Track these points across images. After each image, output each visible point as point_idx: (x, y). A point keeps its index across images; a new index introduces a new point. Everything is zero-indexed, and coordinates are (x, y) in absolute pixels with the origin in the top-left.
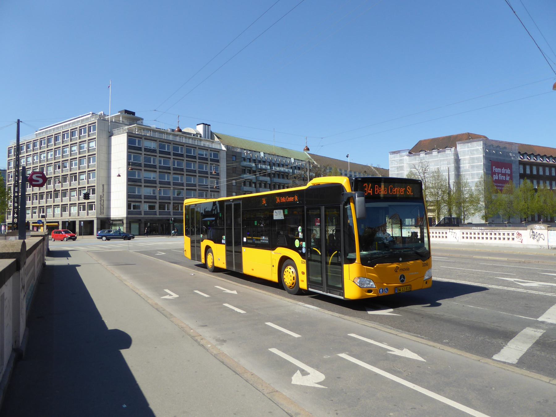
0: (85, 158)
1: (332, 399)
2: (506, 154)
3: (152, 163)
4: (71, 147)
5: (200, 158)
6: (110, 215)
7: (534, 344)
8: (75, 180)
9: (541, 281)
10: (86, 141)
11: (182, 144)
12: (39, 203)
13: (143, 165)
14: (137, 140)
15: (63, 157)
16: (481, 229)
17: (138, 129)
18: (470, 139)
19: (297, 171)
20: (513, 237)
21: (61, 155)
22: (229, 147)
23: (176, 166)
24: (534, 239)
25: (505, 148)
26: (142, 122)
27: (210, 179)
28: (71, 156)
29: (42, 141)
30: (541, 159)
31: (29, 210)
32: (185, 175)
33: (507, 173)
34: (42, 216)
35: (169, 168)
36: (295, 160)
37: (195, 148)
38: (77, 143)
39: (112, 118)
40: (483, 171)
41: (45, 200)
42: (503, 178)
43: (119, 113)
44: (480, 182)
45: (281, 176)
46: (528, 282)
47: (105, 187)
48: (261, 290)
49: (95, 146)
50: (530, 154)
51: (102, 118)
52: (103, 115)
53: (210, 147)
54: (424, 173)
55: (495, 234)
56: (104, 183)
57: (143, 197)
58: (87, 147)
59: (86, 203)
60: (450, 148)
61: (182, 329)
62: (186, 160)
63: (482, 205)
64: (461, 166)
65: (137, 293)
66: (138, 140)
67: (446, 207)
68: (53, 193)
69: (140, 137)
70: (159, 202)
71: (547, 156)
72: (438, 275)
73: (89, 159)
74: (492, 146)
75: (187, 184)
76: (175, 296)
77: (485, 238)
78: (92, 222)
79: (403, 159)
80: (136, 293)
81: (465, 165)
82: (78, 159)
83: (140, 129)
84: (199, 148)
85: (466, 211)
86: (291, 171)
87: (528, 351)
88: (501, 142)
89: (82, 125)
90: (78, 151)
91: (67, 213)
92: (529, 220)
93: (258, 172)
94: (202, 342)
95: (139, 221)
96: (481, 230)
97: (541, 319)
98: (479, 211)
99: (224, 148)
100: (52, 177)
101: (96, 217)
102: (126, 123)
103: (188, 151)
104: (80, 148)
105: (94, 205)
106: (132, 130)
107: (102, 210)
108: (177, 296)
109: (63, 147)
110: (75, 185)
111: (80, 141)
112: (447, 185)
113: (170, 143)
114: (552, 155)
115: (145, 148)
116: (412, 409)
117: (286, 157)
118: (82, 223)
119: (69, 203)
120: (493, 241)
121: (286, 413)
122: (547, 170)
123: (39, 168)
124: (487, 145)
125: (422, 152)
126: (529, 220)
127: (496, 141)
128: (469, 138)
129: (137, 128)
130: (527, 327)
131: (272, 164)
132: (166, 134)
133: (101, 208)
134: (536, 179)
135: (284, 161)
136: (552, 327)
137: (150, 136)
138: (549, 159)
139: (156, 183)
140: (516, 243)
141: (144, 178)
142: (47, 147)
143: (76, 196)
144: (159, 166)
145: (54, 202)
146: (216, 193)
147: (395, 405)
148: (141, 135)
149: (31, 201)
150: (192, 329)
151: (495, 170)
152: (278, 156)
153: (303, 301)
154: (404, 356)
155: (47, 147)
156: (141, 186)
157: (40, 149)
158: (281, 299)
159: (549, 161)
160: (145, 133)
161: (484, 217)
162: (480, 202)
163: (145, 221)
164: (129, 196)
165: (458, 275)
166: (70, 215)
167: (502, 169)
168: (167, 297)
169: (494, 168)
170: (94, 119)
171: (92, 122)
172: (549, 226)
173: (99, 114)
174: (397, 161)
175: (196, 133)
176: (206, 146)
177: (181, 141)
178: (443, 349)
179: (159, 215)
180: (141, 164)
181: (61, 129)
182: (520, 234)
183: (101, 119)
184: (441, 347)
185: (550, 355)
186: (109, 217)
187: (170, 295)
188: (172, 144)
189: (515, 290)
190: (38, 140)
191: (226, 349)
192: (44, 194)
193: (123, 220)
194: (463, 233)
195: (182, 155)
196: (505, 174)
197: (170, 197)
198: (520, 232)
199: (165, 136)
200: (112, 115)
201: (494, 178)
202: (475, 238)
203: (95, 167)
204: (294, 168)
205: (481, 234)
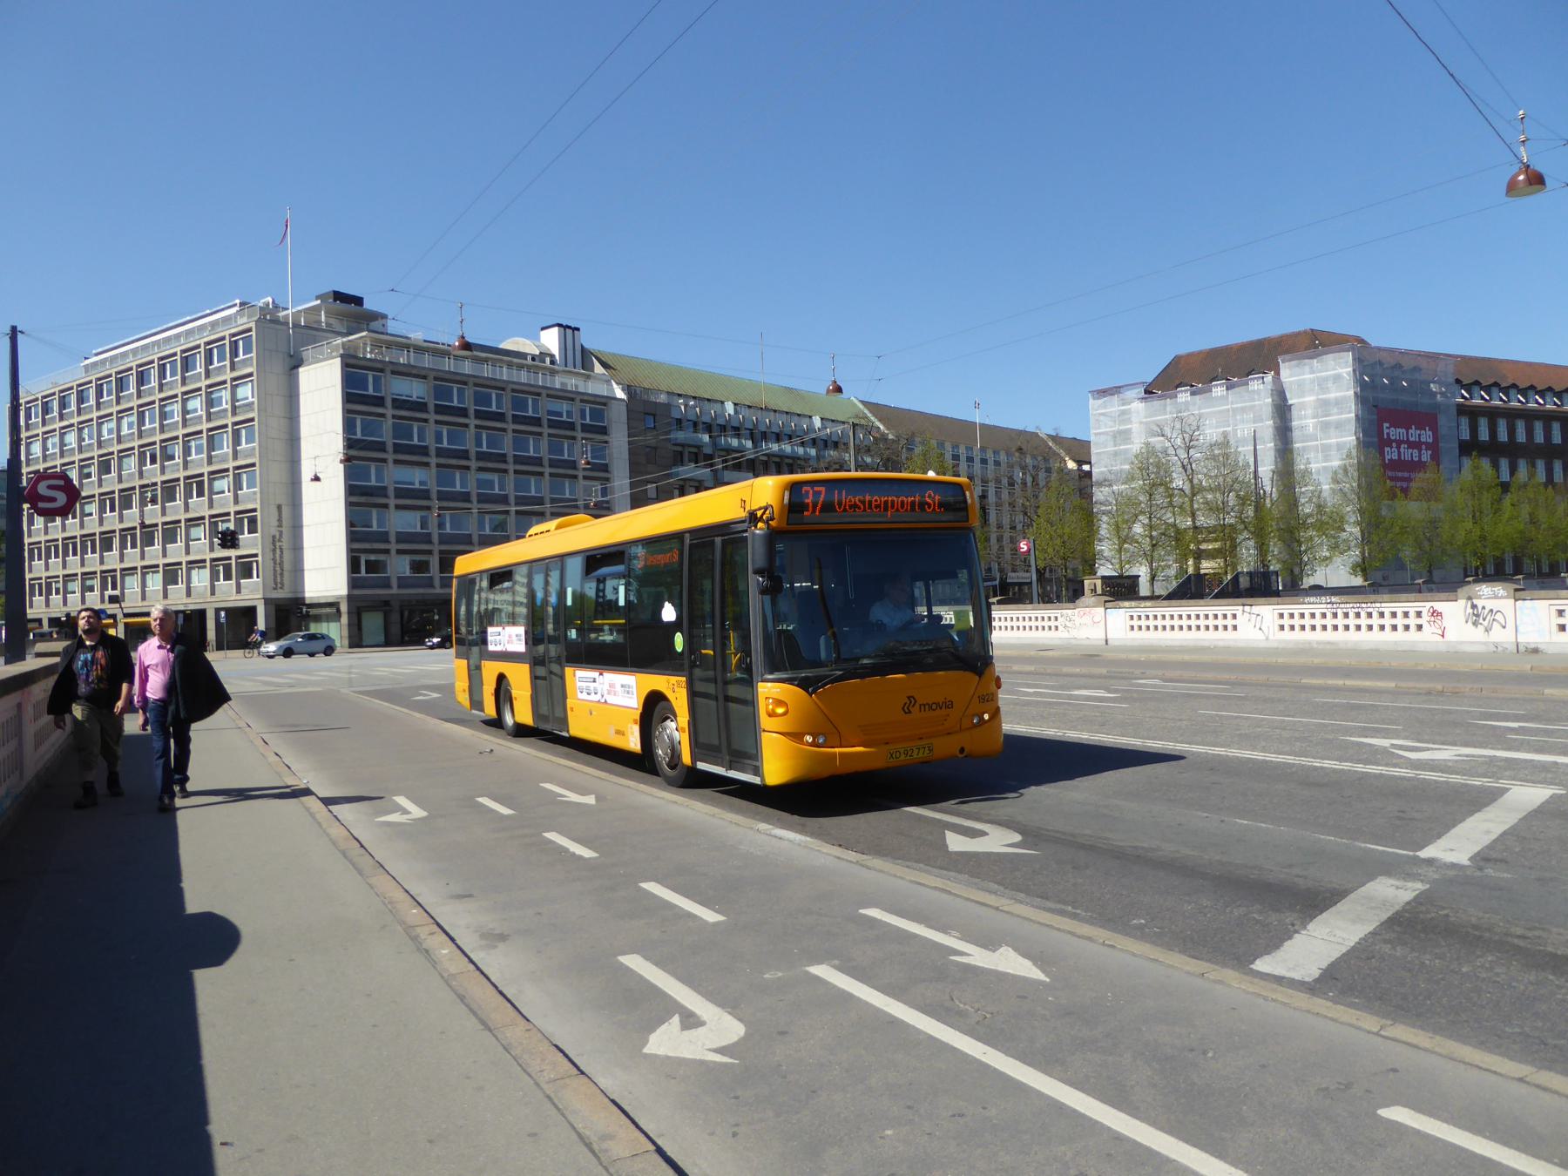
0: (226, 432)
2: (1420, 387)
3: (416, 441)
4: (185, 402)
5: (552, 424)
6: (304, 592)
7: (1382, 924)
8: (201, 494)
9: (1466, 745)
10: (224, 382)
11: (499, 384)
12: (102, 562)
13: (390, 448)
14: (370, 375)
15: (162, 430)
16: (1329, 601)
17: (372, 345)
18: (1316, 347)
19: (832, 452)
20: (1419, 621)
21: (157, 425)
22: (635, 391)
24: (1477, 626)
25: (1416, 369)
26: (384, 325)
27: (582, 482)
28: (185, 425)
29: (102, 385)
30: (1521, 399)
31: (74, 580)
32: (511, 472)
33: (1422, 440)
34: (110, 597)
35: (464, 455)
37: (539, 394)
38: (199, 389)
39: (297, 315)
40: (1354, 438)
41: (118, 553)
42: (1412, 457)
43: (317, 299)
44: (1345, 470)
46: (1428, 749)
47: (286, 511)
49: (253, 397)
50: (1544, 390)
51: (268, 317)
52: (271, 307)
54: (1189, 448)
55: (1370, 615)
56: (282, 498)
57: (393, 538)
58: (229, 397)
59: (234, 559)
60: (1261, 375)
61: (389, 906)
62: (514, 431)
63: (1351, 533)
64: (1293, 423)
66: (373, 375)
67: (1251, 543)
68: (138, 531)
69: (378, 368)
70: (441, 552)
71: (1502, 386)
72: (1181, 735)
73: (236, 434)
74: (1381, 363)
77: (1388, 628)
78: (251, 611)
79: (1130, 409)
81: (1304, 422)
82: (204, 435)
83: (377, 345)
84: (548, 396)
85: (1306, 551)
86: (813, 452)
87: (1358, 946)
89: (213, 337)
90: (204, 413)
91: (182, 586)
92: (1488, 573)
95: (384, 605)
96: (1329, 606)
97: (1426, 853)
98: (1345, 551)
99: (620, 394)
100: (134, 488)
101: (261, 596)
103: (519, 404)
104: (210, 403)
105: (255, 564)
106: (356, 349)
107: (279, 576)
108: (424, 814)
109: (162, 400)
110: (199, 506)
111: (209, 382)
112: (1253, 481)
114: (1535, 384)
116: (953, 1118)
117: (799, 415)
118: (223, 614)
119: (184, 559)
120: (1364, 635)
122: (1538, 428)
123: (96, 464)
124: (1366, 363)
125: (1183, 388)
126: (1488, 573)
127: (1391, 351)
128: (1314, 343)
129: (369, 343)
130: (1380, 877)
131: (758, 435)
133: (275, 570)
134: (1506, 457)
135: (793, 424)
136: (1452, 873)
137: (409, 365)
138: (1543, 397)
140: (1428, 638)
141: (396, 483)
142: (118, 403)
143: (203, 540)
144: (437, 448)
145: (143, 558)
147: (909, 1107)
148: (381, 361)
149: (78, 557)
151: (1388, 434)
152: (775, 411)
154: (993, 968)
155: (118, 403)
156: (386, 506)
157: (98, 408)
158: (714, 816)
159: (1542, 402)
160: (394, 356)
161: (1358, 569)
162: (1346, 526)
165: (1240, 735)
166: (189, 594)
167: (1410, 431)
168: (394, 818)
169: (1387, 428)
170: (245, 320)
171: (240, 328)
172: (1518, 587)
174: (1111, 417)
175: (541, 353)
176: (569, 388)
177: (498, 378)
179: (399, 587)
181: (156, 351)
182: (1440, 614)
183: (265, 318)
184: (1109, 939)
185: (1417, 954)
186: (299, 596)
187: (405, 812)
188: (471, 384)
189: (1383, 772)
190: (90, 382)
192: (115, 536)
193: (338, 603)
194: (1281, 616)
195: (500, 417)
196: (1416, 445)
198: (1439, 606)
199: (449, 363)
200: (297, 306)
201: (1388, 457)
202: (1303, 628)
204: (821, 444)
205: (1329, 615)
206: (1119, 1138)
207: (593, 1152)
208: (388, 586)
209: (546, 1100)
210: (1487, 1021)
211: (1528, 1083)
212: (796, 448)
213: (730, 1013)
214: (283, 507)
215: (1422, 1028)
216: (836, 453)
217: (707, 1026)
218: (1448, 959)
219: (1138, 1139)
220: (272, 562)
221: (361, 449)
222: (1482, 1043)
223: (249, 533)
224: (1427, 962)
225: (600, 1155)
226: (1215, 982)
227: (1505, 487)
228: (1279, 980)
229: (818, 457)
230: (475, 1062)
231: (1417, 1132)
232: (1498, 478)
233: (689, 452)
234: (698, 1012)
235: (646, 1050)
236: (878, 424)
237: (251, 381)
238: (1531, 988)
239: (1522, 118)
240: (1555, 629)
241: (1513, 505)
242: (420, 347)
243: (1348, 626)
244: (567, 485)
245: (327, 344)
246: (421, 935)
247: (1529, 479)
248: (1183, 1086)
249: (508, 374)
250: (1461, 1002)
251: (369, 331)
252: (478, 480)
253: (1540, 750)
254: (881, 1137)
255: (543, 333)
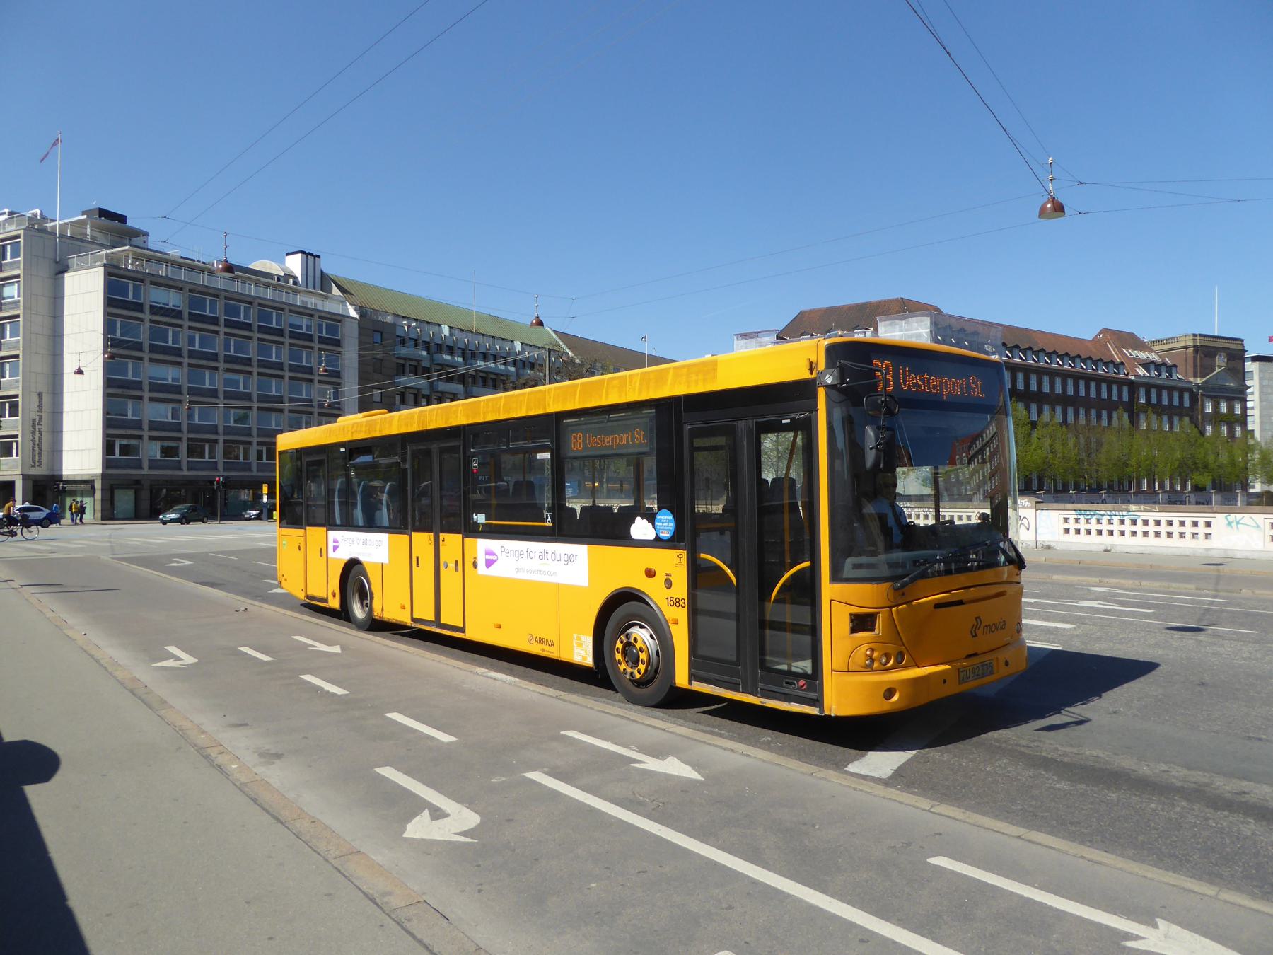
1: (480, 863)
5: (293, 336)
6: (61, 470)
17: (133, 258)
18: (904, 312)
22: (366, 311)
23: (232, 353)
25: (976, 333)
26: (145, 242)
27: (317, 385)
30: (1047, 360)
32: (255, 374)
35: (214, 357)
36: (524, 346)
37: (282, 310)
45: (490, 382)
47: (45, 398)
48: (457, 660)
49: (19, 296)
51: (36, 227)
52: (39, 217)
53: (318, 308)
56: (42, 387)
57: (146, 427)
61: (180, 733)
65: (92, 657)
69: (139, 278)
70: (189, 439)
71: (1059, 354)
74: (950, 327)
75: (259, 395)
76: (472, 819)
77: (1094, 532)
80: (89, 655)
83: (138, 258)
88: (969, 321)
93: (435, 372)
94: (221, 760)
95: (136, 484)
99: (353, 313)
102: (101, 242)
103: (264, 316)
105: (14, 444)
113: (217, 296)
115: (151, 306)
117: (503, 339)
121: (365, 894)
124: (939, 326)
129: (130, 256)
131: (469, 354)
132: (206, 273)
134: (1060, 405)
139: (180, 393)
141: (150, 378)
144: (189, 350)
146: (304, 417)
147: (607, 868)
150: (203, 732)
152: (483, 335)
153: (492, 665)
156: (141, 398)
159: (1061, 363)
160: (153, 268)
161: (928, 482)
163: (151, 485)
164: (108, 423)
170: (13, 227)
173: (29, 214)
176: (309, 306)
177: (247, 293)
178: (749, 755)
180: (141, 344)
185: (957, 759)
186: (56, 473)
187: (178, 659)
188: (222, 297)
191: (277, 776)
195: (248, 327)
197: (216, 426)
200: (64, 218)
203: (19, 347)
204: (520, 364)
206: (755, 882)
207: (376, 904)
208: (140, 467)
209: (335, 871)
210: (1001, 802)
211: (1023, 839)
212: (499, 366)
213: (468, 808)
214: (43, 394)
215: (958, 807)
216: (532, 372)
217: (451, 816)
218: (977, 762)
219: (768, 883)
220: (31, 443)
221: (162, 315)
222: (997, 816)
223: (10, 416)
224: (964, 764)
225: (383, 907)
226: (820, 778)
227: (1034, 425)
228: (864, 777)
229: (518, 375)
230: (274, 846)
231: (952, 872)
232: (1029, 418)
233: (410, 365)
234: (443, 807)
235: (405, 835)
236: (568, 351)
237: (18, 282)
238: (1030, 779)
239: (1051, 163)
240: (1062, 531)
241: (1039, 439)
242: (176, 262)
243: (1069, 529)
244: (274, 384)
245: (91, 254)
246: (212, 754)
247: (1050, 420)
248: (798, 848)
249: (256, 292)
250: (985, 791)
251: (131, 246)
252: (225, 379)
253: (1047, 619)
254: (589, 889)
255: (289, 259)
